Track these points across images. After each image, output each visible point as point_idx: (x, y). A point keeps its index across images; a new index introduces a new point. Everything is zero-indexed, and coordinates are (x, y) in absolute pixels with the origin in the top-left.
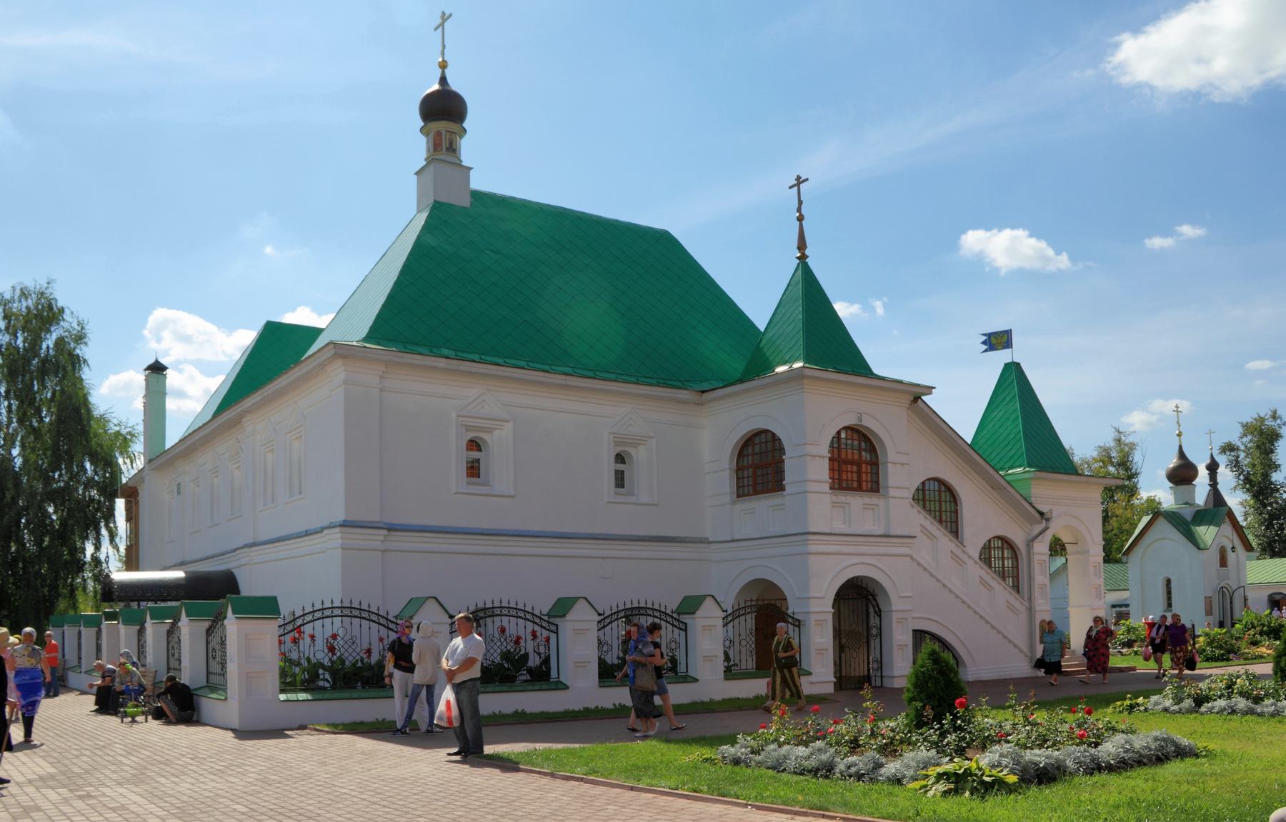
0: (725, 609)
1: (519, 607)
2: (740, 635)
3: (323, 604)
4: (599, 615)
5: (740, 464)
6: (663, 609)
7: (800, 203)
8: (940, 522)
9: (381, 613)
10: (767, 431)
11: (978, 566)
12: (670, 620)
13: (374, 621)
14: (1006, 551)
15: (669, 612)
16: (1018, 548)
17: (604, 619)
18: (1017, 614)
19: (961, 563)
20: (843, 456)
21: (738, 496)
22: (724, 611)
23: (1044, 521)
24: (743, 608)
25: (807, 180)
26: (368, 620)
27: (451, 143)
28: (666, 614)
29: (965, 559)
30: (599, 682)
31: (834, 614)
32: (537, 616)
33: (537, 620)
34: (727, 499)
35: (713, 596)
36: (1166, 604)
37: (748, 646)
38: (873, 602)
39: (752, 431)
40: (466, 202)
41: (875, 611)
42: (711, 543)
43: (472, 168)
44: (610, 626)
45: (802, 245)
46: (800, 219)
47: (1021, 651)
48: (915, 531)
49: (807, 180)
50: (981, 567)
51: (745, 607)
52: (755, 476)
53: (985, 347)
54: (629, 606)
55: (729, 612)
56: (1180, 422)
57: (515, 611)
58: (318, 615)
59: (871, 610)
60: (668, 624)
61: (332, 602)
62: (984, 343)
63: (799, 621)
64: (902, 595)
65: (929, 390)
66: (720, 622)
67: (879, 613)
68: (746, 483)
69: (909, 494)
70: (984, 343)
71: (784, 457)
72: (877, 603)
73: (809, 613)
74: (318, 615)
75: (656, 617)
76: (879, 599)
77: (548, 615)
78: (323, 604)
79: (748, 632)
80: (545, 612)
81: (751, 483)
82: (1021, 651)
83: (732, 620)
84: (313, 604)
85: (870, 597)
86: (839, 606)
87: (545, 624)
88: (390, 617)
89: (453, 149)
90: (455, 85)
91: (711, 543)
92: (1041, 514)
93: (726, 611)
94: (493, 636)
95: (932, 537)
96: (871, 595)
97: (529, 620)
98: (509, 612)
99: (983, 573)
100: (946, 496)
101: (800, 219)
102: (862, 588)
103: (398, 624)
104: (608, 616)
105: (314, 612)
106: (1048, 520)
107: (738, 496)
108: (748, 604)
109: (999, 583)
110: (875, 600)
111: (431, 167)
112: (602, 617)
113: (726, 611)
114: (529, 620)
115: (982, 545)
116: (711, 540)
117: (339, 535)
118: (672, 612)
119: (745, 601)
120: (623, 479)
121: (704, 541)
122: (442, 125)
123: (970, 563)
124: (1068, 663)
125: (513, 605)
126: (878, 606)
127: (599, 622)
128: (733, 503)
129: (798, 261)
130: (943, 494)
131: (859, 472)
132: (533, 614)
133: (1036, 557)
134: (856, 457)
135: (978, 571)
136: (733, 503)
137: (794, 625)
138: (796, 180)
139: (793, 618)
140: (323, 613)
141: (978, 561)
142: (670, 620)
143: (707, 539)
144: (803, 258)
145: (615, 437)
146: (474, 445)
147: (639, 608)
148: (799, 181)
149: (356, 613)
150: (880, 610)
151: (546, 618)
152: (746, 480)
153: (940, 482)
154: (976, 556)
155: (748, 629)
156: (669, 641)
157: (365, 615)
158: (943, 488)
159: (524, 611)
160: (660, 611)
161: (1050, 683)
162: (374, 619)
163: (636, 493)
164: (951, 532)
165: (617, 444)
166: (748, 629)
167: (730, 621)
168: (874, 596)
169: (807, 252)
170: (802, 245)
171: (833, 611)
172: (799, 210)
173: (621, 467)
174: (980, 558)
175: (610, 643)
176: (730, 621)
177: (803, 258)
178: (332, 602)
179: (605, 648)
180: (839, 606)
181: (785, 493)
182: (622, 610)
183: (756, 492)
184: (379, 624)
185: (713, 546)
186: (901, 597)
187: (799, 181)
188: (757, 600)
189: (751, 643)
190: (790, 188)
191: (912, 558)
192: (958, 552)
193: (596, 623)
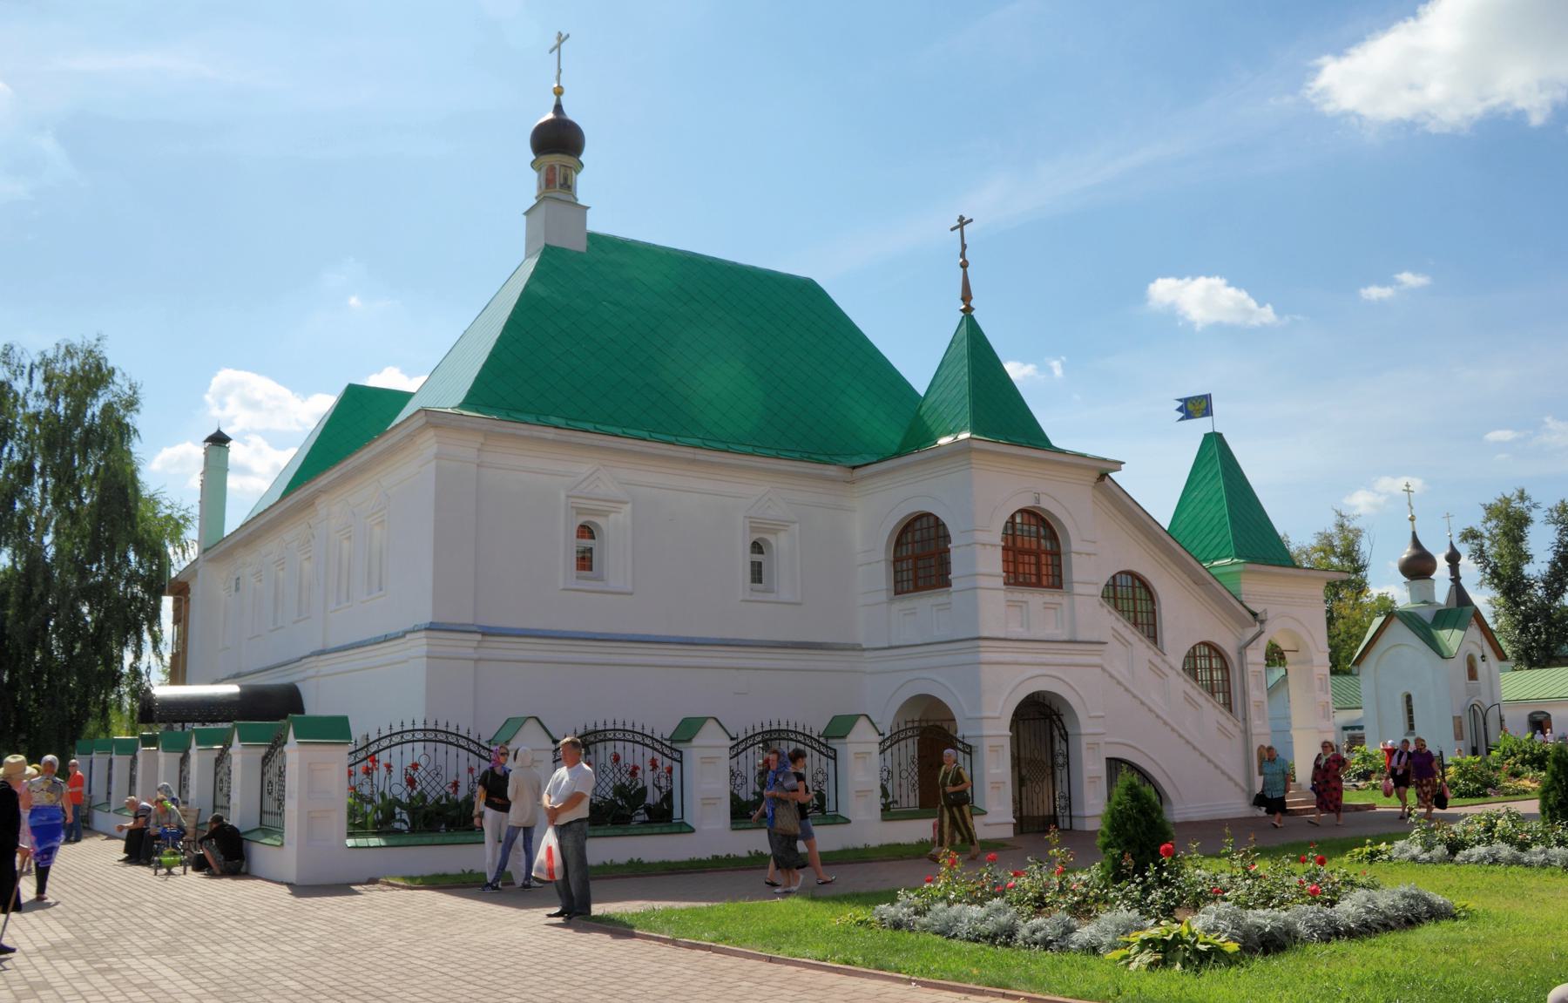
0: (734, 736)
2: (900, 765)
4: (732, 739)
5: (898, 554)
6: (808, 732)
7: (964, 247)
12: (816, 746)
14: (1214, 660)
15: (815, 735)
17: (738, 744)
19: (1161, 674)
20: (1019, 544)
21: (896, 593)
23: (1258, 624)
25: (971, 220)
26: (456, 745)
27: (566, 179)
28: (812, 738)
29: (1166, 669)
31: (1011, 738)
32: (657, 741)
33: (657, 746)
34: (883, 597)
35: (537, 719)
37: (910, 778)
40: (581, 246)
41: (1061, 735)
42: (864, 650)
43: (588, 208)
44: (889, 750)
45: (966, 296)
46: (964, 265)
47: (1236, 784)
49: (971, 220)
50: (1185, 680)
51: (906, 729)
53: (1181, 415)
54: (767, 728)
55: (739, 740)
56: (1412, 504)
58: (396, 739)
59: (1056, 733)
62: (1180, 409)
63: (970, 747)
64: (1092, 714)
65: (1118, 465)
66: (876, 749)
67: (1065, 737)
68: (905, 578)
69: (1098, 590)
70: (1180, 409)
72: (1063, 725)
73: (982, 736)
74: (396, 739)
75: (799, 742)
76: (1065, 719)
77: (671, 739)
78: (414, 724)
79: (910, 761)
80: (667, 736)
81: (911, 577)
82: (1236, 784)
83: (891, 746)
84: (402, 723)
85: (1055, 717)
86: (1017, 727)
87: (667, 751)
88: (483, 742)
89: (568, 186)
90: (571, 114)
91: (864, 650)
92: (1254, 615)
93: (883, 734)
94: (605, 766)
95: (1126, 643)
96: (1056, 714)
97: (647, 745)
98: (436, 736)
99: (1188, 688)
100: (1141, 593)
101: (964, 265)
104: (743, 741)
105: (391, 735)
106: (1262, 622)
107: (896, 593)
108: (910, 725)
110: (1060, 720)
111: (543, 206)
112: (735, 742)
114: (647, 745)
115: (1185, 653)
116: (864, 646)
117: (425, 641)
118: (819, 736)
119: (906, 722)
120: (760, 572)
121: (856, 648)
123: (1172, 674)
125: (629, 727)
127: (880, 744)
128: (891, 601)
129: (962, 314)
130: (1137, 590)
131: (1038, 564)
132: (652, 738)
133: (1251, 668)
134: (1034, 546)
135: (1181, 684)
136: (891, 601)
137: (964, 752)
138: (959, 220)
139: (963, 743)
140: (402, 737)
141: (1182, 672)
142: (816, 746)
143: (860, 645)
144: (968, 310)
146: (586, 531)
147: (787, 731)
148: (962, 222)
149: (441, 737)
150: (1066, 733)
151: (668, 743)
152: (905, 578)
153: (1134, 576)
157: (638, 738)
158: (1137, 583)
159: (643, 734)
160: (804, 735)
162: (463, 744)
165: (753, 530)
167: (888, 747)
169: (973, 304)
170: (966, 296)
172: (963, 255)
173: (758, 558)
177: (968, 310)
180: (1017, 727)
181: (951, 589)
182: (759, 734)
183: (917, 588)
184: (469, 750)
186: (1090, 717)
187: (962, 222)
188: (920, 721)
189: (913, 774)
191: (1104, 669)
192: (1157, 661)
193: (877, 746)
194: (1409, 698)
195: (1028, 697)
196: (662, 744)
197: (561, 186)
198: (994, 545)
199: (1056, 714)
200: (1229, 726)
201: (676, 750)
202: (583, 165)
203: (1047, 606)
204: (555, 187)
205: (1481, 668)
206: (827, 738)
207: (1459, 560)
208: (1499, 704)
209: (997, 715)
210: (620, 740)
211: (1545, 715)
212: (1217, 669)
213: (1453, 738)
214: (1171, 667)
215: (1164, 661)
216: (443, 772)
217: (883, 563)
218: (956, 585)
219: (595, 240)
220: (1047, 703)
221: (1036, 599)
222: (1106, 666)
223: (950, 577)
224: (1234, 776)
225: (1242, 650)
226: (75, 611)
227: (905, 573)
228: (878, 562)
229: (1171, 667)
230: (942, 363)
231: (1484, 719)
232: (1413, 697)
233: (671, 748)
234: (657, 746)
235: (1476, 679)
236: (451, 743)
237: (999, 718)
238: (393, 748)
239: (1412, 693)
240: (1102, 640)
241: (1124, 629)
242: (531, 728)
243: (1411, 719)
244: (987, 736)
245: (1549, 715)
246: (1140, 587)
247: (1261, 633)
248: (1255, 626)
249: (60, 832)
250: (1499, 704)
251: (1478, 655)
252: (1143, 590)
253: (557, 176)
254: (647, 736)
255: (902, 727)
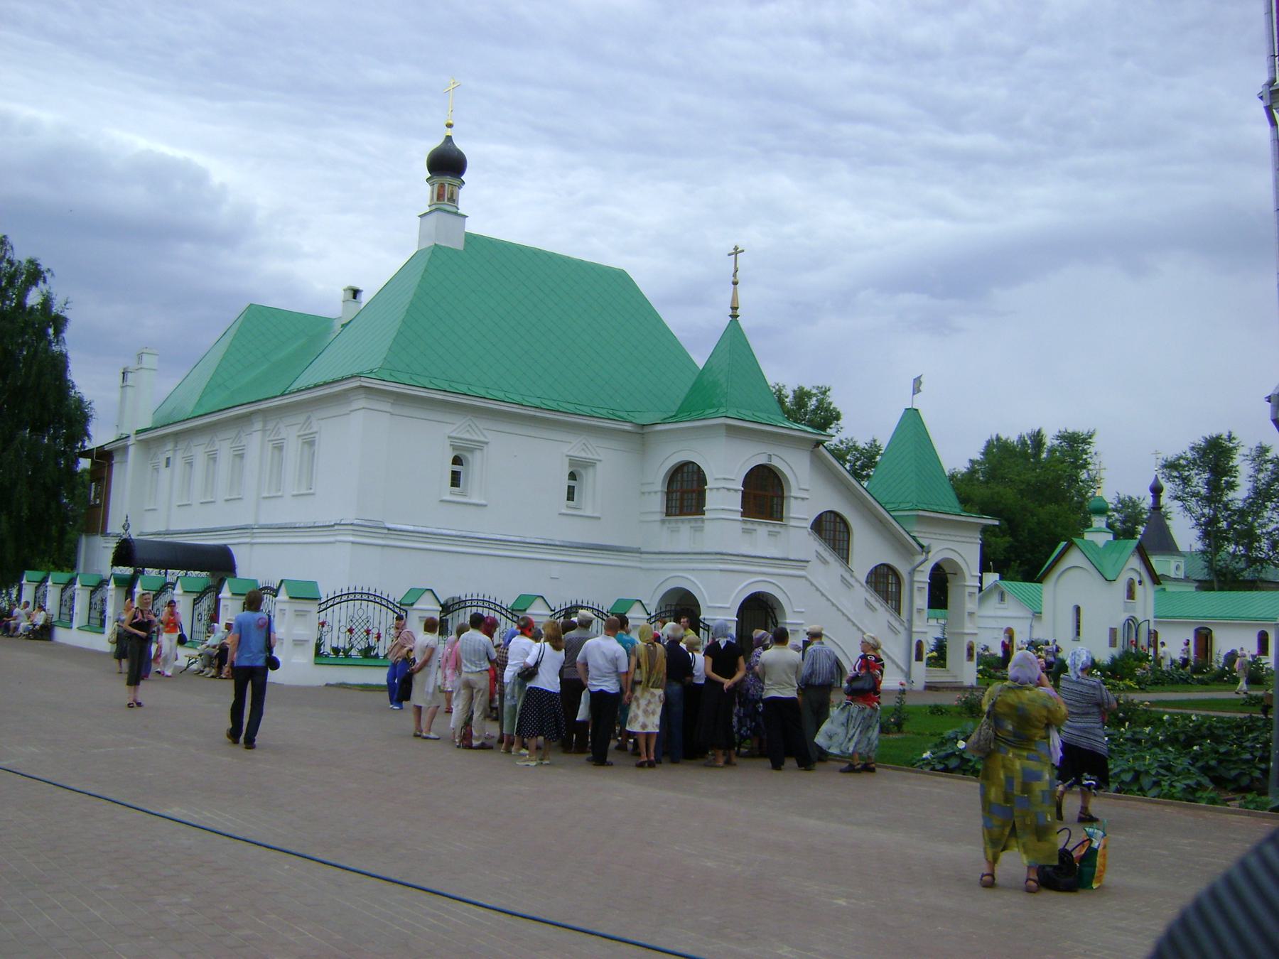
0: (553, 609)
1: (377, 594)
2: (340, 621)
3: (355, 589)
4: (648, 614)
6: (600, 609)
8: (834, 549)
9: (503, 606)
10: (693, 463)
11: (863, 589)
13: (384, 605)
15: (605, 611)
16: (903, 578)
17: (554, 614)
18: (896, 634)
19: (849, 585)
22: (552, 610)
23: (924, 553)
24: (345, 594)
25: (743, 251)
27: (452, 194)
28: (602, 613)
29: (851, 581)
30: (315, 660)
32: (504, 609)
33: (504, 612)
34: (658, 517)
36: (1075, 633)
38: (771, 614)
39: (679, 462)
40: (460, 246)
43: (467, 217)
47: (898, 666)
48: (811, 556)
49: (743, 251)
50: (867, 591)
51: (666, 611)
52: (682, 499)
55: (556, 611)
57: (353, 596)
58: (351, 597)
59: (770, 621)
60: (502, 616)
61: (362, 589)
63: (708, 626)
64: (795, 610)
68: (674, 505)
69: (808, 524)
71: (706, 487)
72: (775, 615)
74: (345, 598)
76: (777, 612)
78: (355, 589)
79: (349, 620)
80: (509, 606)
81: (678, 505)
82: (898, 666)
83: (655, 622)
85: (769, 610)
86: (743, 615)
87: (509, 616)
89: (453, 199)
90: (460, 144)
92: (922, 547)
93: (554, 611)
94: (353, 617)
95: (825, 562)
96: (770, 608)
100: (840, 526)
102: (759, 599)
103: (604, 620)
104: (557, 612)
105: (342, 595)
106: (928, 553)
107: (667, 514)
108: (668, 608)
109: (881, 605)
111: (435, 215)
112: (553, 613)
113: (554, 611)
116: (643, 550)
118: (608, 612)
122: (448, 180)
123: (857, 585)
124: (354, 652)
125: (486, 599)
126: (775, 617)
128: (663, 521)
129: (731, 319)
132: (501, 607)
133: (916, 585)
135: (862, 593)
137: (704, 629)
139: (704, 623)
141: (865, 584)
145: (570, 459)
149: (371, 598)
150: (777, 621)
151: (398, 605)
153: (836, 514)
154: (863, 579)
155: (348, 616)
156: (388, 627)
158: (838, 520)
161: (157, 672)
163: (583, 507)
164: (843, 558)
165: (571, 465)
166: (348, 616)
167: (653, 622)
168: (773, 609)
171: (737, 619)
172: (735, 275)
173: (572, 483)
174: (867, 582)
175: (331, 624)
176: (653, 622)
177: (734, 317)
178: (362, 589)
179: (325, 629)
180: (743, 615)
181: (704, 517)
183: (681, 513)
184: (388, 607)
185: (643, 556)
186: (794, 612)
187: (737, 251)
190: (729, 255)
192: (847, 576)
194: (1078, 609)
195: (751, 594)
196: (507, 611)
197: (449, 200)
198: (736, 491)
199: (770, 608)
200: (896, 624)
201: (515, 615)
202: (464, 183)
203: (771, 534)
204: (444, 200)
205: (1138, 590)
206: (401, 604)
207: (1161, 492)
208: (1149, 621)
209: (728, 605)
210: (486, 607)
211: (1208, 631)
212: (892, 583)
213: (1108, 644)
214: (857, 580)
215: (852, 576)
216: (371, 621)
217: (659, 495)
218: (707, 515)
219: (471, 239)
220: (765, 600)
221: (762, 529)
222: (809, 577)
223: (704, 508)
224: (897, 660)
225: (913, 572)
226: (1144, 718)
227: (674, 509)
228: (656, 492)
229: (857, 580)
230: (712, 353)
231: (1137, 631)
232: (1081, 609)
233: (512, 614)
234: (504, 612)
235: (1133, 599)
236: (491, 609)
237: (729, 608)
238: (349, 602)
239: (1080, 606)
240: (808, 559)
241: (824, 552)
242: (539, 602)
243: (1078, 627)
244: (968, 634)
245: (1211, 631)
246: (840, 523)
247: (926, 560)
248: (922, 554)
249: (572, 621)
250: (1149, 621)
251: (1137, 579)
252: (842, 525)
253: (446, 192)
254: (498, 605)
255: (663, 609)
